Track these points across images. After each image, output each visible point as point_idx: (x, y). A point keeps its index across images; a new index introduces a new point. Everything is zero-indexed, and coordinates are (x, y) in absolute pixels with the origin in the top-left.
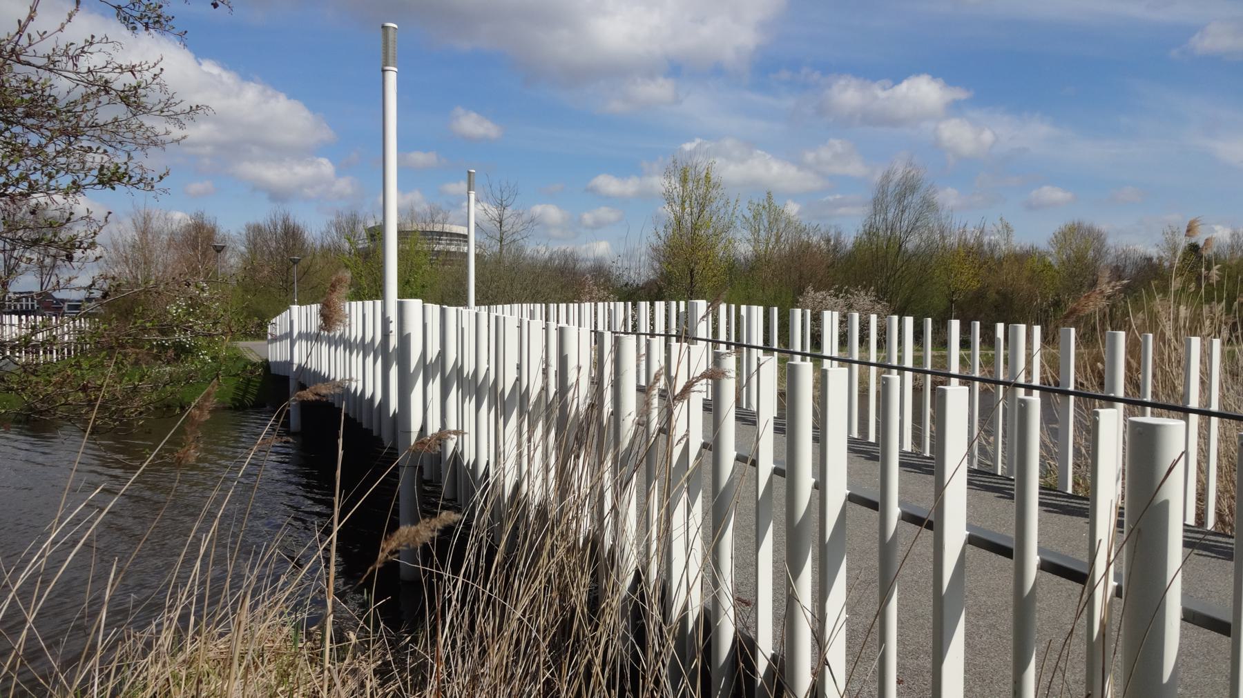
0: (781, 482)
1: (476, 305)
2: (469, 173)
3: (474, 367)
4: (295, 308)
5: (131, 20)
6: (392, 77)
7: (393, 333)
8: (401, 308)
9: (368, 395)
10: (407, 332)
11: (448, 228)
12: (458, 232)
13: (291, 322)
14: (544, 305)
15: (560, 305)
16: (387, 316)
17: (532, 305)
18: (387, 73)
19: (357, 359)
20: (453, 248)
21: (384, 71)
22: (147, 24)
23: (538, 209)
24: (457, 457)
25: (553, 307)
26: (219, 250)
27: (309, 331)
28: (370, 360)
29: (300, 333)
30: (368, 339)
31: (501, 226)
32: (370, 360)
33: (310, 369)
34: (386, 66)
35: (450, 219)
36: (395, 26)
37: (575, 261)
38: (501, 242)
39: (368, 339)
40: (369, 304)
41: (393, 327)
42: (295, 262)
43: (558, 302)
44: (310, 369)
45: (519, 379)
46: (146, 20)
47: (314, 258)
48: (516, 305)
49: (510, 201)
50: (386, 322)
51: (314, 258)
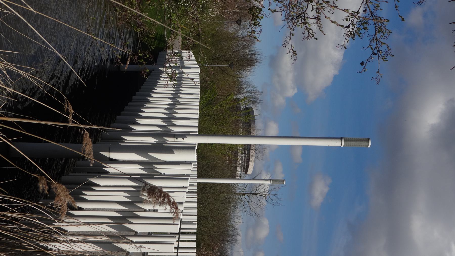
0: (133, 233)
1: (198, 183)
2: (284, 181)
3: (178, 125)
4: (199, 71)
5: (351, 19)
6: (337, 143)
7: (176, 140)
8: (189, 148)
9: (139, 121)
10: (175, 152)
11: (252, 159)
12: (250, 166)
13: (189, 68)
14: (196, 231)
15: (195, 243)
16: (187, 137)
17: (196, 223)
18: (340, 140)
19: (161, 113)
20: (239, 162)
21: (341, 139)
22: (349, 27)
23: (266, 222)
24: (90, 186)
25: (194, 237)
26: (238, 22)
27: (184, 79)
28: (160, 122)
29: (183, 73)
30: (175, 122)
31: (253, 194)
32: (160, 122)
33: (160, 80)
34: (345, 140)
35: (257, 161)
36: (369, 146)
37: (231, 241)
38: (242, 194)
39: (175, 122)
40: (196, 123)
41: (180, 140)
42: (230, 65)
43: (198, 242)
44: (160, 80)
45: (136, 234)
46: (351, 27)
47: (233, 76)
48: (196, 211)
49: (269, 200)
50: (184, 135)
51: (233, 76)
